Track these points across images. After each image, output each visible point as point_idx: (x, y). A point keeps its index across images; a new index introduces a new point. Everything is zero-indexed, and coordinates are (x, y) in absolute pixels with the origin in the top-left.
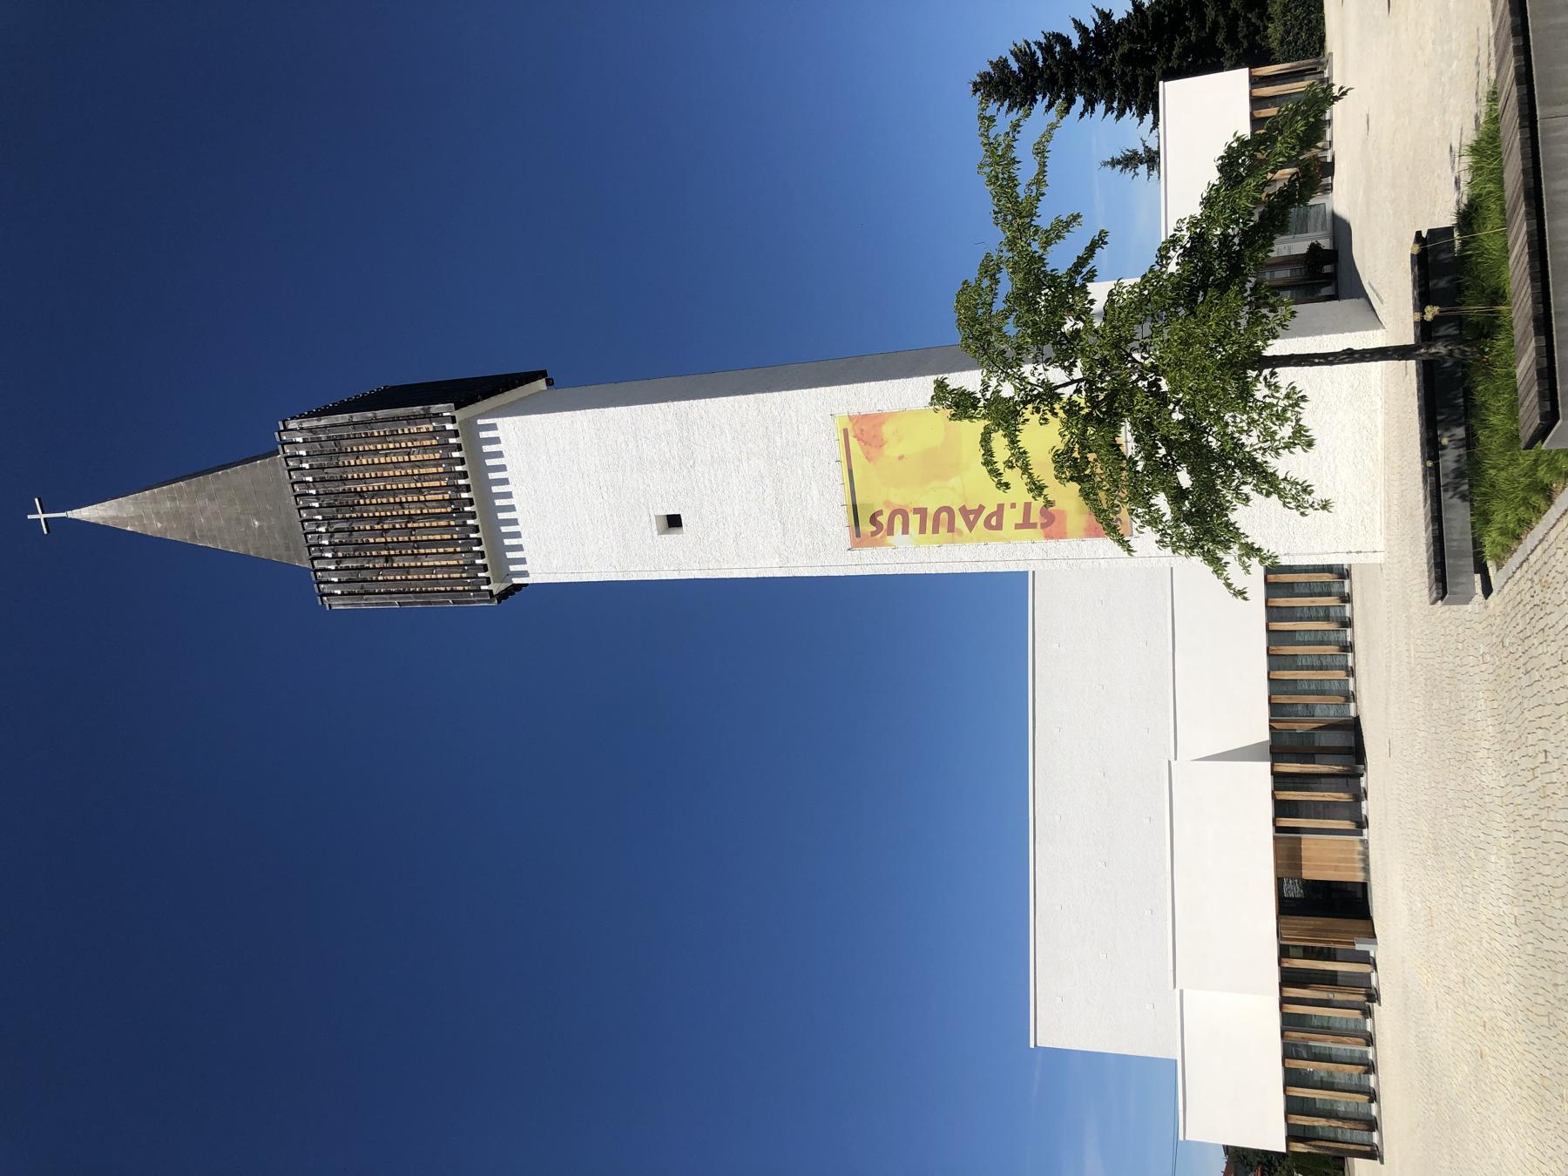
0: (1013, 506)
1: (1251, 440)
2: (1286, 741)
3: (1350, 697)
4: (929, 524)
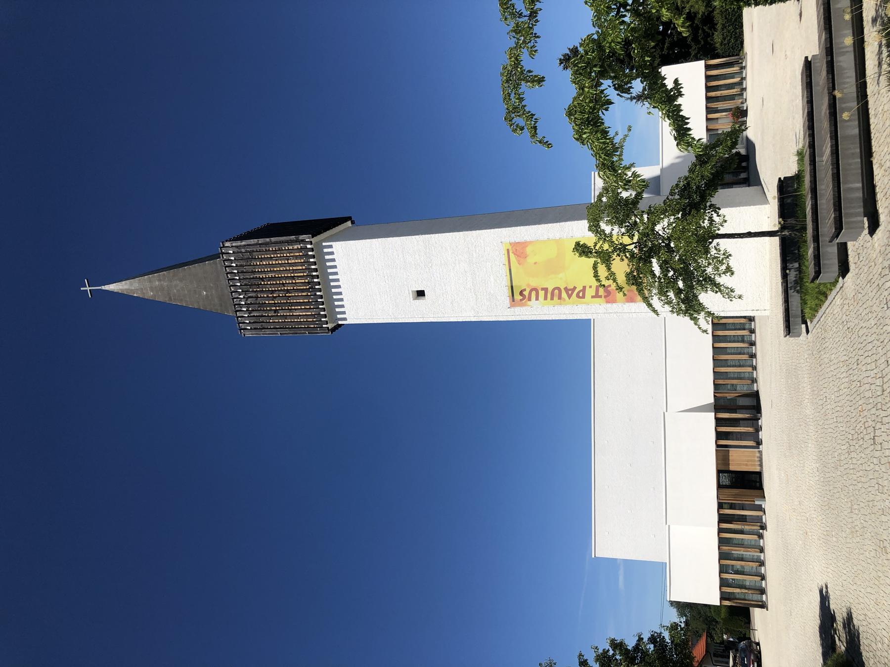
0: (591, 287)
1: (709, 270)
2: (722, 402)
3: (754, 381)
4: (549, 296)
